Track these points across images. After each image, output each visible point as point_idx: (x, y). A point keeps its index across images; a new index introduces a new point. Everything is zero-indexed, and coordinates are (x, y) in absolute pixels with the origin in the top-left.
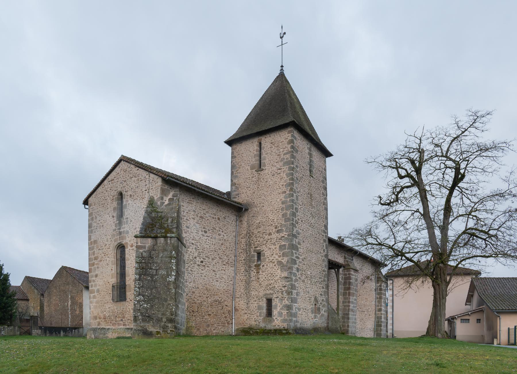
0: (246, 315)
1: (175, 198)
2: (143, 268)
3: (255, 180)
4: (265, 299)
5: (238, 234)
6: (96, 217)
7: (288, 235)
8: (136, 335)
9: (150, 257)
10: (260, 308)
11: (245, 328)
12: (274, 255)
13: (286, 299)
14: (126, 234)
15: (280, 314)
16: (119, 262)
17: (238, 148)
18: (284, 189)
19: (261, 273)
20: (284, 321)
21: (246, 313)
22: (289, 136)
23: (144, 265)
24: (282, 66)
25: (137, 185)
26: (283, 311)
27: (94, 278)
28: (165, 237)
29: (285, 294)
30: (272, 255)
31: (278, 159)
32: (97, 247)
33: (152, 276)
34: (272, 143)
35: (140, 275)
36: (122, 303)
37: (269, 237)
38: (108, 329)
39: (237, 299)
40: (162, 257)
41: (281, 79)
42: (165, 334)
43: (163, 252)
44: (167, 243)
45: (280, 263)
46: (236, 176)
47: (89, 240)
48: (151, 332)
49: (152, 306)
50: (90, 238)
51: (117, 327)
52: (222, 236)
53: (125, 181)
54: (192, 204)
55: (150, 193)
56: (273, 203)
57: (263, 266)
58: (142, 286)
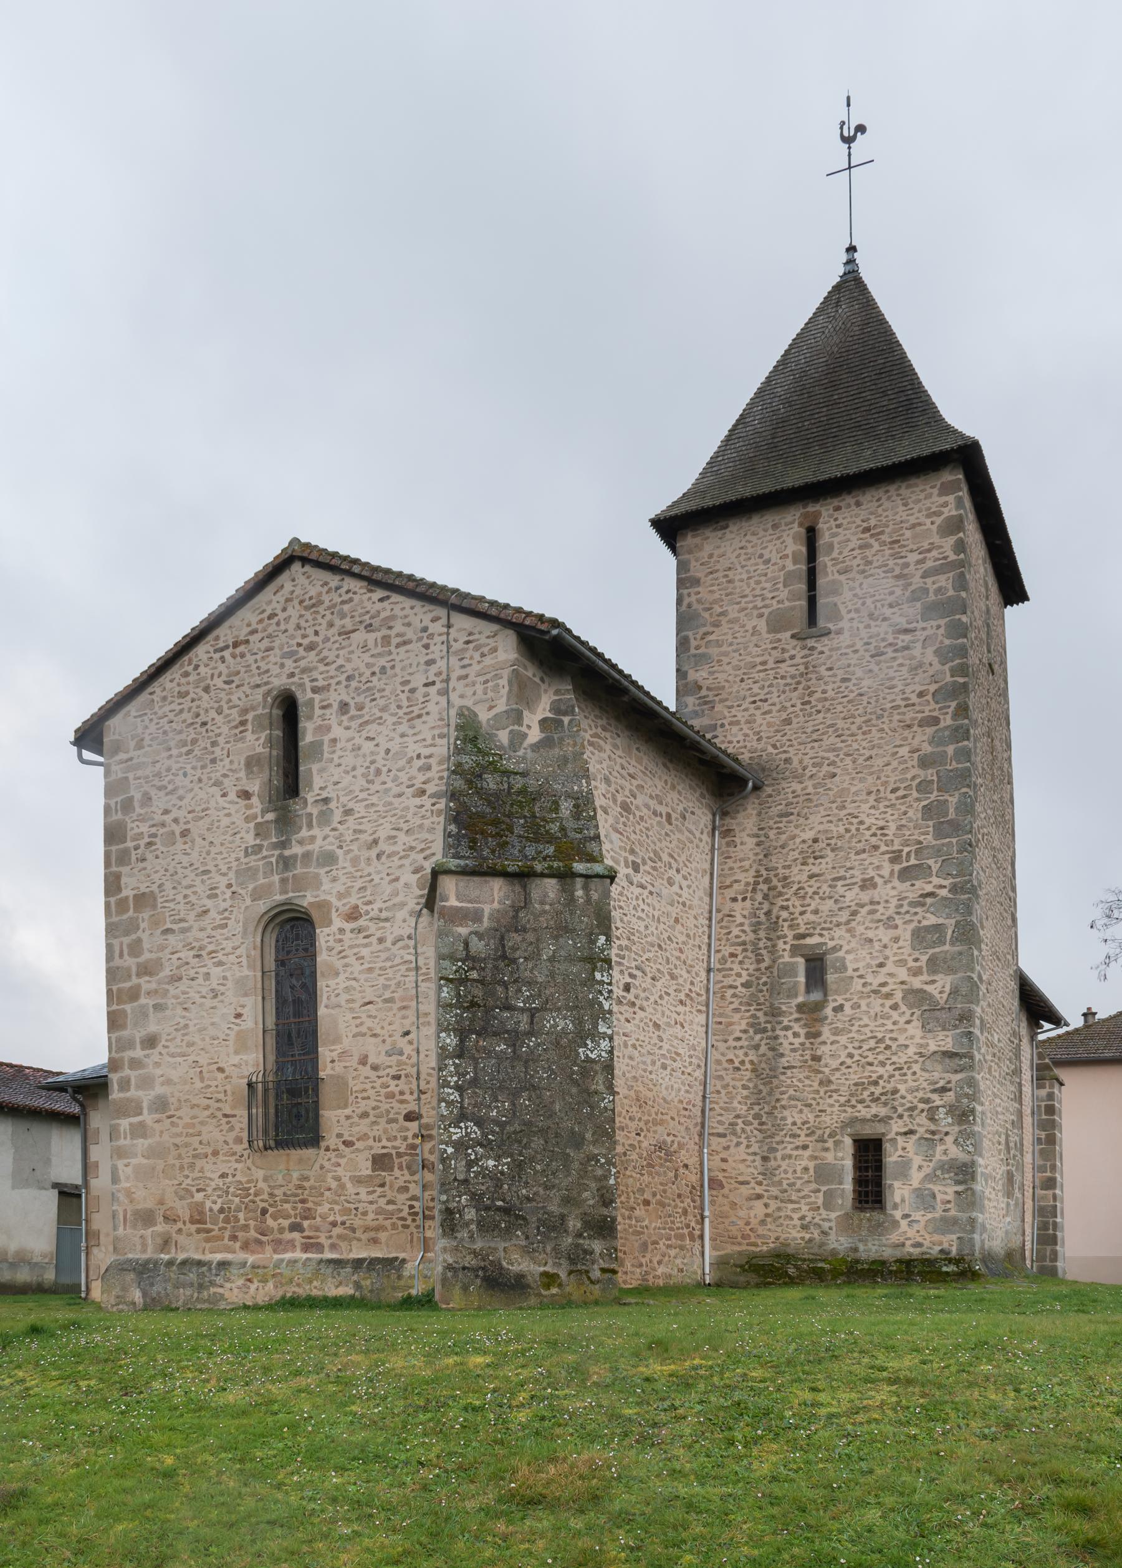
0: (759, 1204)
1: (566, 720)
2: (473, 1004)
3: (792, 670)
4: (848, 1142)
5: (718, 885)
6: (147, 799)
7: (954, 889)
8: (457, 1291)
9: (504, 957)
10: (824, 1174)
11: (755, 1256)
12: (890, 967)
13: (949, 1140)
14: (320, 865)
15: (925, 1199)
16: (272, 984)
17: (708, 548)
18: (930, 708)
19: (826, 1034)
20: (946, 1224)
21: (759, 1197)
22: (945, 504)
23: (478, 992)
24: (852, 249)
25: (382, 662)
26: (936, 1188)
27: (138, 1053)
28: (565, 876)
29: (945, 1121)
30: (881, 965)
31: (898, 592)
32: (155, 923)
33: (515, 1038)
34: (867, 530)
35: (463, 1034)
36: (296, 1154)
37: (865, 897)
38: (223, 1265)
39: (715, 1140)
40: (552, 959)
41: (851, 288)
42: (580, 1284)
43: (556, 938)
44: (572, 900)
45: (917, 998)
46: (703, 655)
47: (108, 893)
48: (520, 1276)
49: (519, 1166)
50: (112, 884)
51: (267, 1256)
52: (676, 888)
53: (311, 647)
54: (601, 749)
55: (454, 697)
56: (879, 762)
57: (839, 1009)
58: (474, 1082)
